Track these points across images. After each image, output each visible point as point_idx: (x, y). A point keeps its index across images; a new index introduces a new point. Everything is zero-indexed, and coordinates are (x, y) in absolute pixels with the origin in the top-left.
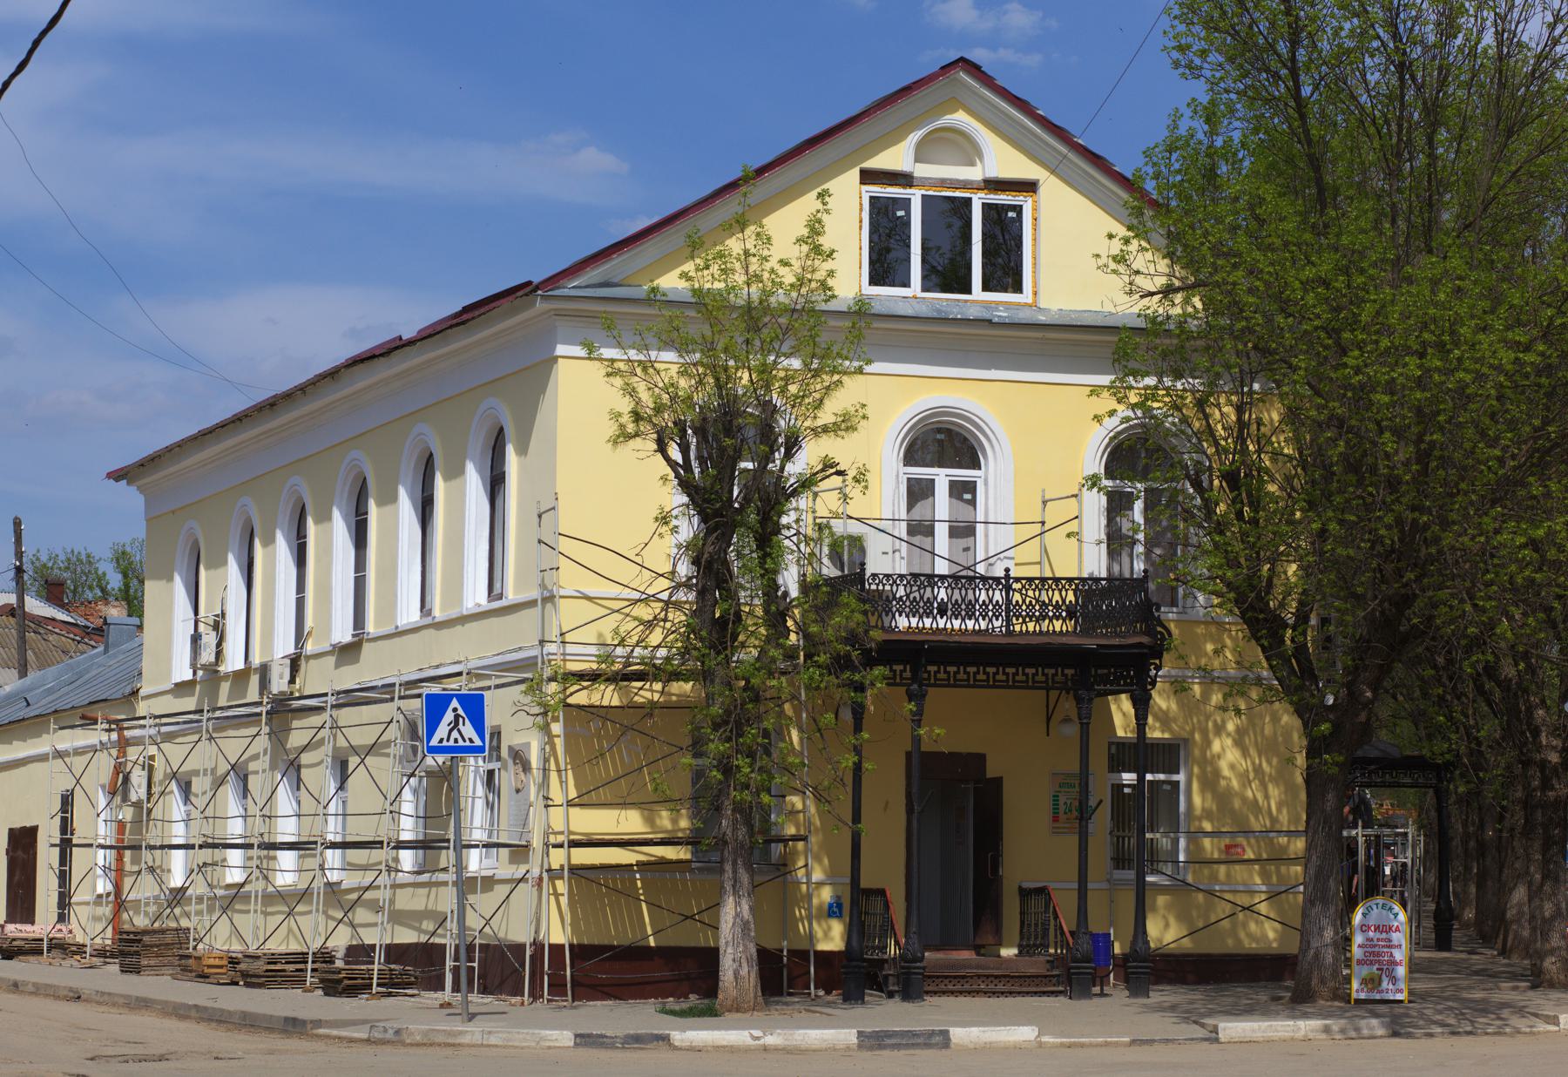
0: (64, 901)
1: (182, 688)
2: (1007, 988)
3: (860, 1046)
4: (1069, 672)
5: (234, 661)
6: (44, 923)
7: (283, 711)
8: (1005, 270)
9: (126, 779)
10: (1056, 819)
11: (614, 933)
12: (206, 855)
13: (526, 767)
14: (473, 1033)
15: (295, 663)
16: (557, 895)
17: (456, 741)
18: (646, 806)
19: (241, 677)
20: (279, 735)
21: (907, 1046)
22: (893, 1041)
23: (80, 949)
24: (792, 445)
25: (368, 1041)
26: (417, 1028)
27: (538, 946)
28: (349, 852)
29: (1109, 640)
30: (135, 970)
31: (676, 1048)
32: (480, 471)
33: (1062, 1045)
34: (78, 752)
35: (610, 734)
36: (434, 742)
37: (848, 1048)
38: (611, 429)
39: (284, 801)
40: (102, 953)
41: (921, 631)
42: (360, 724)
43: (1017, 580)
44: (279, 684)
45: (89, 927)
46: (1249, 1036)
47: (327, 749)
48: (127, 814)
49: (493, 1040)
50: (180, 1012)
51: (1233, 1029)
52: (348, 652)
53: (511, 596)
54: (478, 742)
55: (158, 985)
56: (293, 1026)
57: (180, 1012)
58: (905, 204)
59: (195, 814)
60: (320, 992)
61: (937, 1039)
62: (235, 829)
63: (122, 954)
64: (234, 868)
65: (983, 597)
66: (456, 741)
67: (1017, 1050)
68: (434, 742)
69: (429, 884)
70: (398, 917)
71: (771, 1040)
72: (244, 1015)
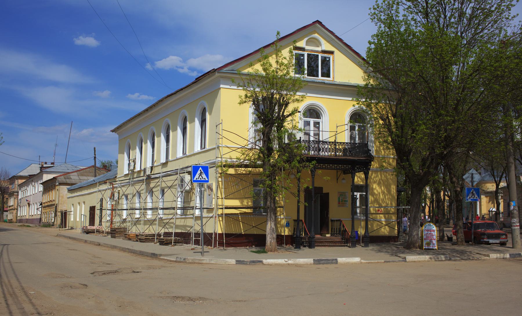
0: (101, 221)
1: (126, 175)
2: (340, 245)
3: (314, 263)
4: (350, 166)
5: (138, 168)
6: (96, 227)
7: (149, 178)
8: (327, 74)
9: (114, 196)
10: (339, 203)
11: (233, 230)
12: (131, 211)
13: (212, 190)
14: (206, 259)
15: (152, 168)
16: (220, 221)
18: (241, 199)
19: (139, 172)
20: (148, 184)
23: (103, 232)
24: (287, 105)
25: (176, 261)
26: (191, 257)
27: (216, 234)
28: (164, 210)
29: (354, 159)
30: (115, 237)
31: (264, 264)
32: (199, 120)
33: (367, 263)
34: (103, 190)
35: (238, 178)
36: (195, 179)
37: (311, 264)
38: (239, 100)
39: (149, 199)
40: (108, 233)
42: (169, 181)
44: (148, 172)
45: (105, 227)
46: (414, 260)
47: (159, 188)
48: (114, 203)
49: (212, 262)
50: (124, 250)
51: (410, 258)
52: (165, 165)
53: (207, 147)
54: (207, 179)
55: (120, 242)
56: (154, 256)
57: (124, 250)
58: (303, 55)
59: (129, 202)
60: (158, 244)
61: (334, 261)
62: (137, 206)
63: (111, 233)
64: (137, 214)
65: (326, 146)
67: (355, 264)
68: (195, 179)
69: (185, 218)
70: (177, 227)
71: (290, 262)
72: (141, 252)
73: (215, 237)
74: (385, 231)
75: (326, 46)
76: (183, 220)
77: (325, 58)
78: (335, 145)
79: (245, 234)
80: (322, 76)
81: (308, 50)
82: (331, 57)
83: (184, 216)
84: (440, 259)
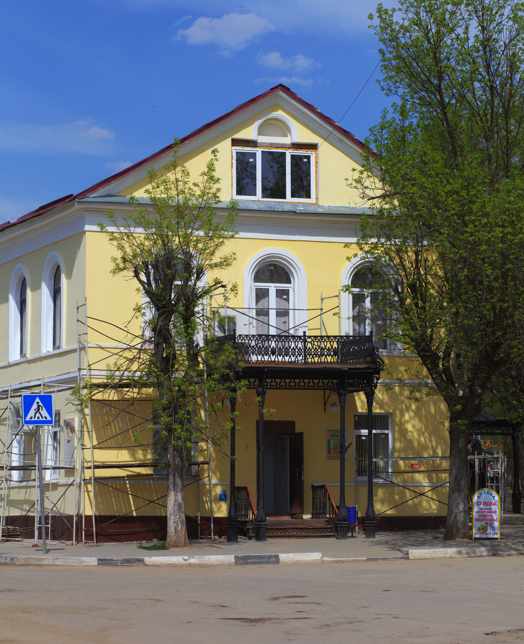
3: (236, 563)
4: (335, 381)
8: (302, 188)
10: (329, 452)
13: (73, 430)
14: (48, 559)
16: (88, 492)
17: (38, 418)
18: (131, 448)
21: (259, 563)
22: (252, 561)
24: (200, 273)
27: (79, 516)
29: (352, 367)
31: (147, 565)
32: (49, 287)
33: (333, 561)
35: (114, 412)
36: (28, 419)
37: (230, 564)
41: (263, 362)
43: (309, 337)
46: (424, 556)
49: (58, 562)
51: (415, 553)
53: (65, 347)
54: (49, 418)
58: (254, 155)
61: (273, 559)
65: (293, 345)
66: (38, 418)
68: (28, 419)
71: (193, 561)
73: (79, 523)
74: (430, 506)
75: (300, 133)
76: (24, 490)
77: (301, 157)
78: (305, 341)
79: (138, 518)
80: (293, 196)
81: (263, 145)
82: (313, 155)
83: (24, 484)
84: (478, 554)
